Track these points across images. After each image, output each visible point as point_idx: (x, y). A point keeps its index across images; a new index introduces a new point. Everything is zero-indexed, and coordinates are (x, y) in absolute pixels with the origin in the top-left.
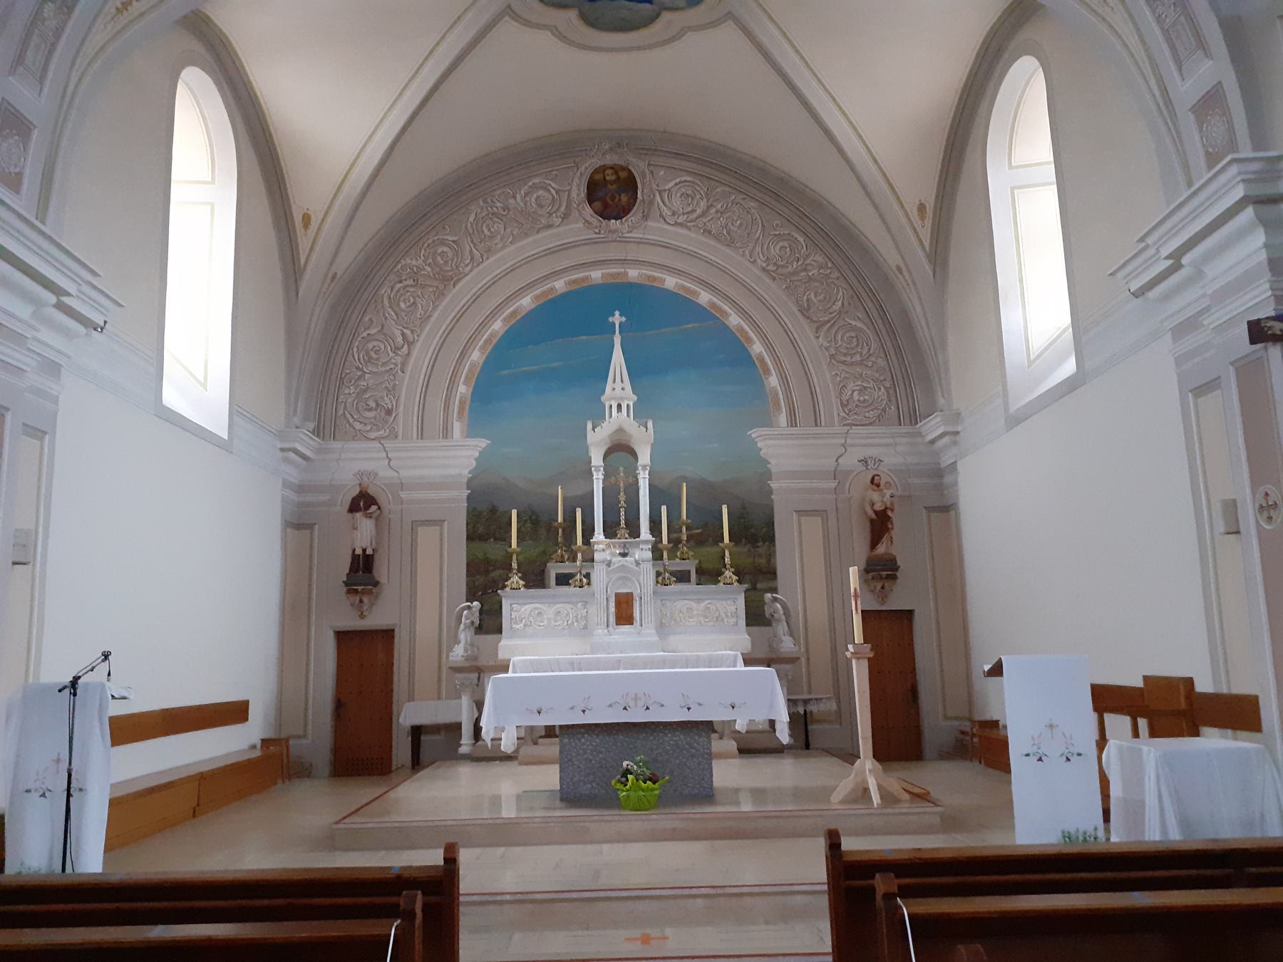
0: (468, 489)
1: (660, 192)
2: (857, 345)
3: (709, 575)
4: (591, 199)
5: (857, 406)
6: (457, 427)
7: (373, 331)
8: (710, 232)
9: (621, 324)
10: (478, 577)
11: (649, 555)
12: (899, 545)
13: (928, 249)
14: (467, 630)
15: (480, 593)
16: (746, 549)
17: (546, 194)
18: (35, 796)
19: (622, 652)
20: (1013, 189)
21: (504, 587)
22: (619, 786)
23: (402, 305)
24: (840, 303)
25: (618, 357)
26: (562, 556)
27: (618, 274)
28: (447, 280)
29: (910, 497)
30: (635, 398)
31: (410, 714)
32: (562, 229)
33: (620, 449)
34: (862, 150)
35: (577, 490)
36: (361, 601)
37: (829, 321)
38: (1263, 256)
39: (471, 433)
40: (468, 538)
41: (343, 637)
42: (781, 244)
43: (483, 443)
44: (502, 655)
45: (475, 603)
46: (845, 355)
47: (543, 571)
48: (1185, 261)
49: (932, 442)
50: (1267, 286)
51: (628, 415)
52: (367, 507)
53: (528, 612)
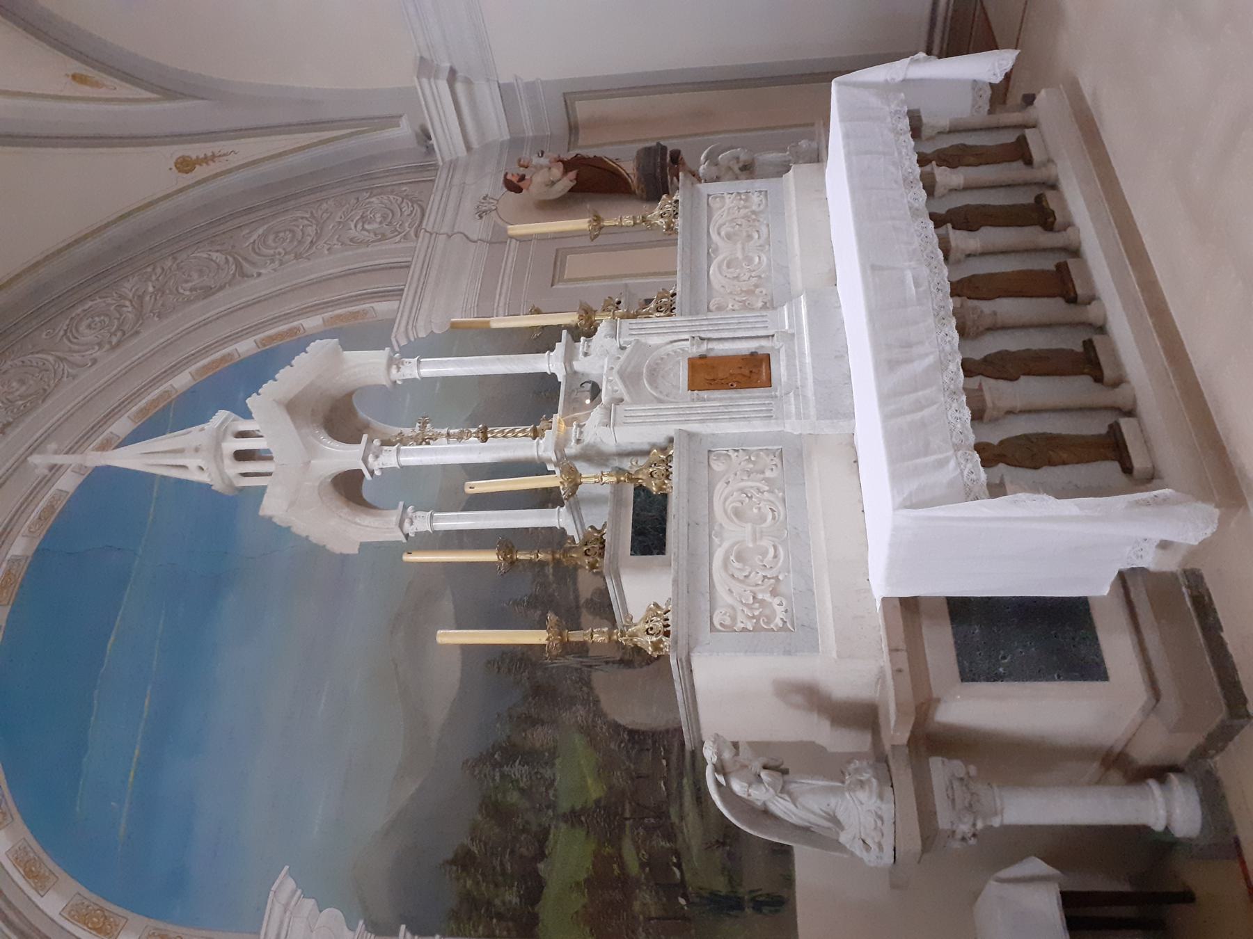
0: (396, 933)
10: (637, 906)
14: (793, 787)
15: (682, 901)
43: (285, 887)
47: (632, 733)
49: (469, 148)
53: (737, 587)
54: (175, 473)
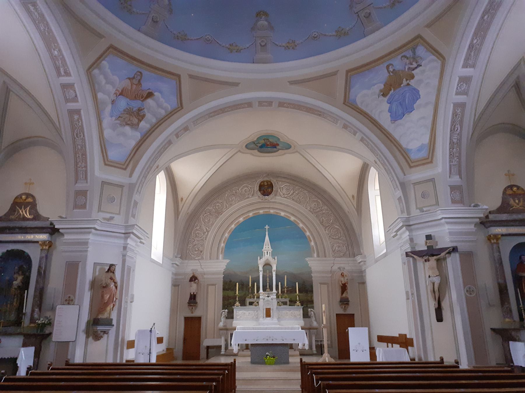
1: (280, 188)
2: (337, 233)
3: (292, 303)
4: (260, 190)
5: (337, 252)
6: (221, 256)
7: (197, 228)
8: (294, 200)
9: (268, 228)
11: (275, 297)
12: (350, 294)
13: (356, 207)
16: (305, 294)
17: (247, 189)
18: (141, 354)
19: (267, 325)
20: (375, 196)
21: (234, 305)
22: (265, 359)
23: (206, 220)
24: (332, 221)
25: (267, 238)
26: (251, 297)
27: (268, 211)
28: (219, 213)
29: (353, 279)
30: (272, 250)
31: (206, 342)
32: (252, 198)
33: (267, 265)
34: (335, 182)
35: (255, 276)
36: (192, 308)
37: (328, 226)
38: (408, 237)
39: (224, 258)
40: (223, 289)
41: (186, 319)
42: (315, 203)
43: (228, 261)
44: (234, 325)
45: (226, 310)
46: (333, 236)
48: (398, 233)
49: (360, 263)
50: (409, 245)
51: (270, 255)
52: (195, 280)
54: (265, 244)
